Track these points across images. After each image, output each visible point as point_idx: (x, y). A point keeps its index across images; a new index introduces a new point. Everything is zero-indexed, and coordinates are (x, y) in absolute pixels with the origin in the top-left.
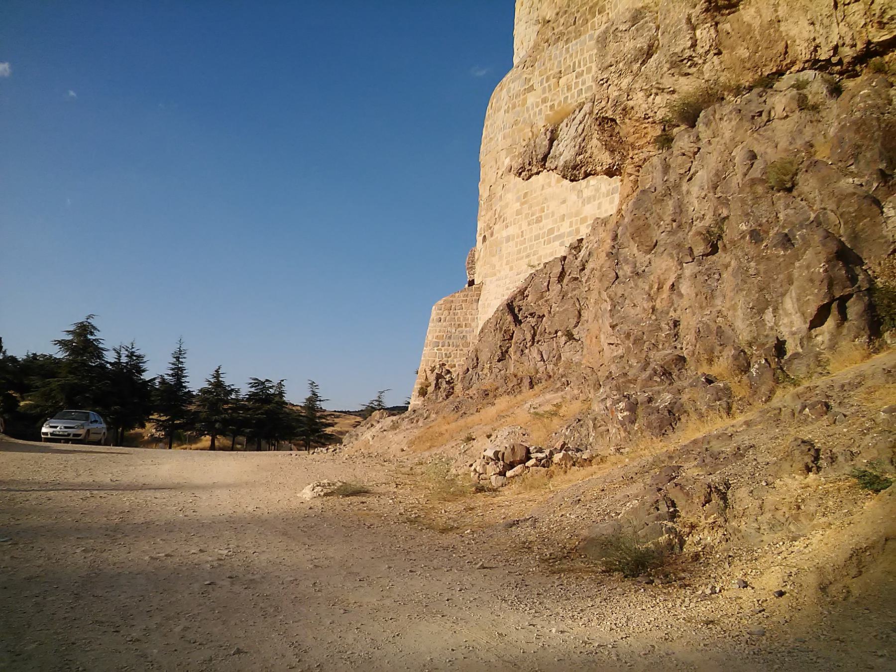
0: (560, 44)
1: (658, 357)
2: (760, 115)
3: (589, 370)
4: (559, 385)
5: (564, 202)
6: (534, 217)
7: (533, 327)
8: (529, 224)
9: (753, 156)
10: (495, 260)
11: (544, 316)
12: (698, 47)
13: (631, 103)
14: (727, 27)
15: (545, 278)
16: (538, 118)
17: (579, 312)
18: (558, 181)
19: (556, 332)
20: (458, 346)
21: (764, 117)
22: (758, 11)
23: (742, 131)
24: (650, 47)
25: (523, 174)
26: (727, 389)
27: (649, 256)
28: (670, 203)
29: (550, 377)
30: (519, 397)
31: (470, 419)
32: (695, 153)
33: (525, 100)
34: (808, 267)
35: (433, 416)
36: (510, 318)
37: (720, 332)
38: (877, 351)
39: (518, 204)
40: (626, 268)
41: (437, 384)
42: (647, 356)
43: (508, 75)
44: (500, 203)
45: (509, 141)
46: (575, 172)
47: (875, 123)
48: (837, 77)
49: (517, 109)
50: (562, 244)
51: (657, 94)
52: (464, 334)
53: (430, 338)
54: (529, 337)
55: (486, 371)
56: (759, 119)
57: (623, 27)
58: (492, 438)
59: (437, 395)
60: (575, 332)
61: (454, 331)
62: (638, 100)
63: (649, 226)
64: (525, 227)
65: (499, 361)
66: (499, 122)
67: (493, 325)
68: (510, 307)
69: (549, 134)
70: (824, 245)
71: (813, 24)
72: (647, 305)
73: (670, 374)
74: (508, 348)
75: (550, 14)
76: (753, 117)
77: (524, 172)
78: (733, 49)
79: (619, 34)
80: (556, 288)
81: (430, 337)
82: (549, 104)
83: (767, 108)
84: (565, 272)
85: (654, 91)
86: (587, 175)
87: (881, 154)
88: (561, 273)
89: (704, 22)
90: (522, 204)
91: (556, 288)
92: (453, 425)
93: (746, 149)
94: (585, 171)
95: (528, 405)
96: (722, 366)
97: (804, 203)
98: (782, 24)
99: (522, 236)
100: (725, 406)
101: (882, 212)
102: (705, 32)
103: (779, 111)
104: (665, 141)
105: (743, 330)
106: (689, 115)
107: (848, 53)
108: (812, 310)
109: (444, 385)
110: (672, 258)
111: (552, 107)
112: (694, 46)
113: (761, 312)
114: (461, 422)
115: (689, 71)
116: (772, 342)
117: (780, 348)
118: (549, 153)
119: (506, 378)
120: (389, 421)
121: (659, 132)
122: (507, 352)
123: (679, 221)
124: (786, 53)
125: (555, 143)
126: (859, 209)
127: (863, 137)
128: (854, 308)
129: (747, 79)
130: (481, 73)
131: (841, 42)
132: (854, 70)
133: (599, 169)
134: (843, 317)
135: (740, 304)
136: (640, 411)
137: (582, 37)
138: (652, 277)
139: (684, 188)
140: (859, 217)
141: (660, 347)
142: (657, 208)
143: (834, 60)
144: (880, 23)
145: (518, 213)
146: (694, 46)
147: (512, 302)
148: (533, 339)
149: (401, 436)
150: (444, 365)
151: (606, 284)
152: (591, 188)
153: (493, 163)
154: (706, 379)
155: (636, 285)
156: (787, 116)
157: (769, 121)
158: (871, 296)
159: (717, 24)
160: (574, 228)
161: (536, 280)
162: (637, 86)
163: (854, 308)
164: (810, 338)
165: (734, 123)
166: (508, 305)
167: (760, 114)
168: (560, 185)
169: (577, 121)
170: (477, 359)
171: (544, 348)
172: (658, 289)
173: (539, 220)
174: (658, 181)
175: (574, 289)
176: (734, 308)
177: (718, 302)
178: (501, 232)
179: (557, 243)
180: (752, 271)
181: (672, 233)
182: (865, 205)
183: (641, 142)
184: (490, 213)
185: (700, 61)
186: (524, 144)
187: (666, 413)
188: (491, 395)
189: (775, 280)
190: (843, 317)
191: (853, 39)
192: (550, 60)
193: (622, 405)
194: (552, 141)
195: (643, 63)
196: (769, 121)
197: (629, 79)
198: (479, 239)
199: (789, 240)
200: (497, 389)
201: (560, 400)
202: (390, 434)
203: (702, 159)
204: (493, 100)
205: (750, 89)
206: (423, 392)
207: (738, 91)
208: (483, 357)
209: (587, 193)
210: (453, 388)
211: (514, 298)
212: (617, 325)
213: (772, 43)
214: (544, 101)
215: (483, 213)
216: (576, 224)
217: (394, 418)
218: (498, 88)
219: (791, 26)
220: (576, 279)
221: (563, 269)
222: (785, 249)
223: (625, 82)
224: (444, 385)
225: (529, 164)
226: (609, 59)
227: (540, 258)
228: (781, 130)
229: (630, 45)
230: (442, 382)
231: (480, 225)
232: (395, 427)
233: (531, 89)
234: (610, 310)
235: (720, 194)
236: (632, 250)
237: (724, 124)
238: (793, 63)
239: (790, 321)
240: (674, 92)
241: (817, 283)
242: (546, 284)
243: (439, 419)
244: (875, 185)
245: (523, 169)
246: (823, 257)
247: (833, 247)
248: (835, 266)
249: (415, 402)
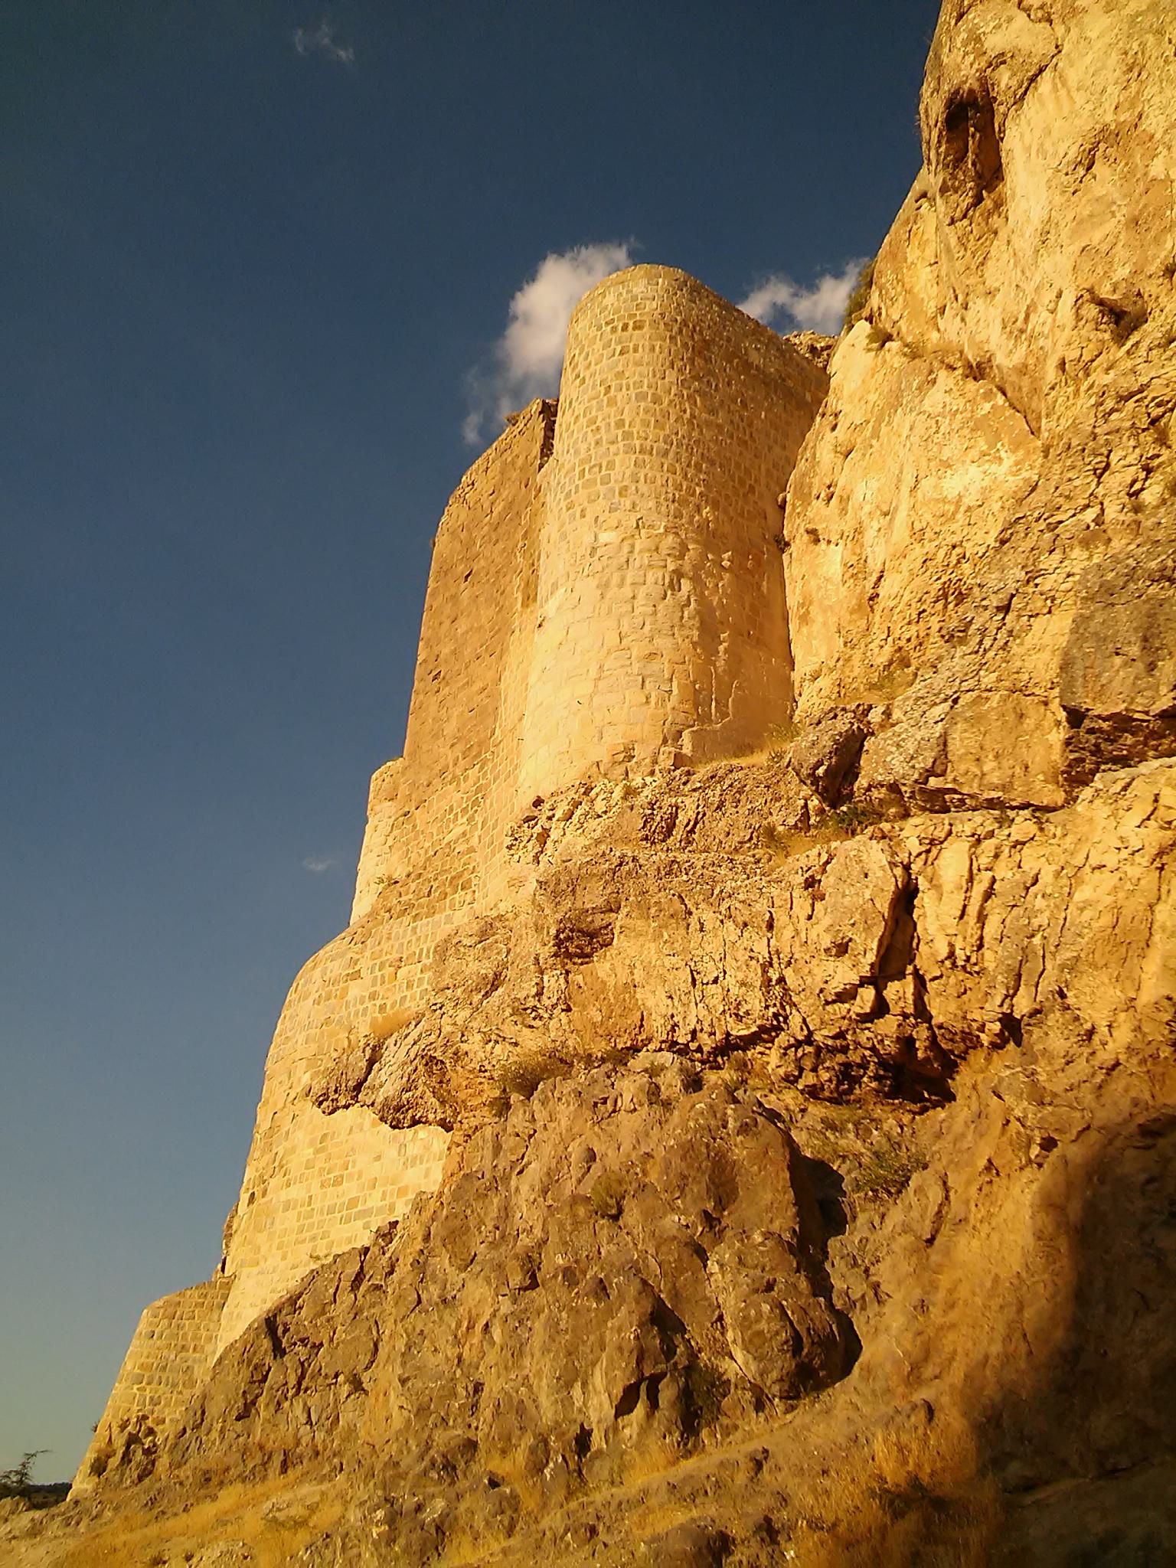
0: (406, 919)
1: (442, 1439)
2: (605, 1103)
3: (366, 1448)
4: (327, 1469)
5: (378, 1158)
6: (332, 1176)
7: (302, 1364)
8: (322, 1186)
9: (591, 1156)
10: (261, 1238)
11: (321, 1345)
12: (544, 997)
13: (465, 1047)
14: (579, 978)
15: (332, 1280)
16: (361, 1019)
17: (376, 1345)
18: (374, 1125)
19: (336, 1376)
20: (175, 1385)
21: (609, 1105)
22: (613, 969)
23: (581, 1121)
24: (497, 976)
25: (325, 1104)
26: (514, 1496)
27: (463, 1275)
28: (495, 1201)
29: (317, 1454)
30: (260, 1488)
31: (171, 1524)
32: (530, 1136)
33: (345, 991)
34: (620, 1330)
35: (108, 1514)
36: (267, 1343)
37: (521, 1410)
38: (688, 1454)
39: (311, 1150)
40: (431, 1288)
41: (126, 1454)
42: (430, 1436)
43: (328, 948)
44: (285, 1144)
45: (313, 1048)
46: (399, 1115)
47: (704, 1150)
48: (698, 1066)
49: (333, 1001)
50: (366, 1226)
51: (497, 1042)
52: (189, 1363)
53: (129, 1367)
54: (292, 1381)
55: (214, 1434)
56: (602, 1108)
57: (467, 942)
58: (195, 1560)
59: (122, 1475)
60: (365, 1378)
61: (172, 1357)
62: (473, 1043)
63: (468, 1229)
64: (315, 1189)
65: (238, 1419)
66: (303, 1015)
67: (237, 1354)
68: (270, 1324)
69: (368, 1051)
70: (638, 1303)
71: (671, 997)
72: (452, 1352)
73: (454, 1468)
74: (257, 1397)
75: (399, 873)
76: (596, 1104)
77: (328, 1101)
78: (584, 1007)
79: (462, 950)
80: (346, 1299)
81: (130, 1365)
82: (378, 1003)
83: (613, 1094)
84: (361, 1273)
85: (494, 1037)
86: (415, 1122)
87: (708, 1189)
88: (358, 1274)
89: (553, 967)
90: (317, 1151)
91: (346, 1299)
92: (136, 1536)
93: (584, 1146)
94: (413, 1117)
95: (269, 1504)
96: (513, 1464)
97: (629, 1238)
98: (638, 990)
99: (309, 1204)
100: (506, 1523)
101: (705, 1266)
102: (553, 980)
103: (625, 1103)
104: (502, 1107)
105: (547, 1411)
106: (527, 1082)
107: (707, 1042)
108: (618, 1391)
109: (139, 1456)
110: (489, 1283)
111: (382, 1008)
112: (539, 994)
113: (569, 1385)
114: (153, 1530)
115: (533, 1023)
116: (576, 1429)
117: (583, 1440)
118: (366, 1080)
119: (244, 1452)
120: (26, 1519)
121: (497, 1093)
122: (254, 1403)
123: (503, 1234)
124: (642, 1026)
125: (376, 1066)
126: (680, 1259)
127: (690, 1166)
128: (667, 1393)
129: (599, 1048)
130: (320, 867)
131: (698, 1028)
132: (716, 1061)
133: (431, 1117)
134: (654, 1404)
135: (546, 1370)
136: (404, 1525)
137: (437, 917)
138: (461, 1309)
139: (513, 1183)
140: (680, 1270)
141: (451, 1423)
142: (478, 1206)
143: (693, 1046)
144: (737, 1015)
145: (309, 1165)
146: (539, 994)
147: (275, 1316)
148: (299, 1383)
149: (42, 1551)
150: (145, 1418)
151: (403, 1311)
152: (418, 1143)
153: (285, 1077)
154: (490, 1480)
155: (441, 1318)
156: (635, 1110)
157: (614, 1111)
158: (688, 1377)
159: (568, 972)
160: (387, 1202)
161: (319, 1282)
162: (475, 1024)
163: (667, 1393)
164: (616, 1430)
165: (572, 1108)
166: (267, 1320)
167: (605, 1101)
168: (376, 1130)
169: (410, 1040)
170: (203, 1413)
171: (314, 1401)
172: (468, 1329)
173: (338, 1182)
174: (488, 1164)
175: (373, 1305)
176: (539, 1374)
177: (527, 1362)
178: (278, 1193)
179: (360, 1223)
180: (563, 1325)
181: (494, 1245)
182: (687, 1253)
183: (475, 1102)
184: (268, 1157)
185: (546, 1016)
186: (335, 1055)
187: (433, 1531)
188: (215, 1481)
189: (584, 1342)
190: (654, 1404)
191: (712, 1025)
192: (389, 939)
193: (380, 1514)
194: (371, 1063)
195: (486, 995)
196: (614, 1111)
197: (467, 1012)
198: (245, 1197)
199: (604, 1289)
200: (227, 1469)
201: (317, 1498)
202: (22, 1547)
203: (537, 1147)
204: (300, 980)
205: (603, 1060)
206: (99, 1468)
207: (589, 1060)
208: (214, 1410)
209: (413, 1150)
210: (153, 1463)
211: (279, 1309)
212: (408, 1379)
213: (626, 1011)
214: (373, 996)
215: (257, 1154)
216: (392, 1194)
217: (37, 1514)
218: (309, 964)
219: (649, 995)
220: (378, 1287)
221: (362, 1267)
222: (598, 1300)
223: (463, 1014)
224: (139, 1456)
225: (336, 1091)
226: (447, 981)
227: (330, 1245)
228: (628, 1124)
229: (477, 967)
230: (134, 1453)
231: (250, 1174)
232: (35, 1531)
233: (356, 975)
234: (403, 1354)
235: (550, 1202)
236: (442, 1262)
237: (561, 1107)
238: (650, 1040)
239: (596, 1403)
240: (516, 1044)
241: (626, 1354)
242: (331, 1291)
243: (117, 1522)
244: (700, 1229)
245: (326, 1096)
246: (635, 1317)
247: (647, 1305)
248: (649, 1332)
249: (82, 1484)
